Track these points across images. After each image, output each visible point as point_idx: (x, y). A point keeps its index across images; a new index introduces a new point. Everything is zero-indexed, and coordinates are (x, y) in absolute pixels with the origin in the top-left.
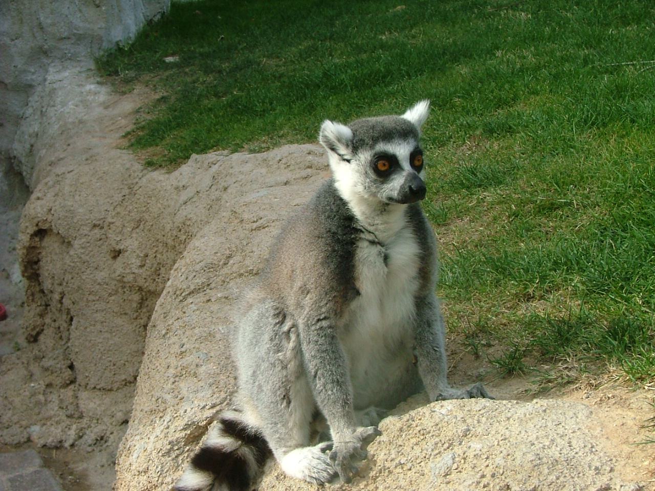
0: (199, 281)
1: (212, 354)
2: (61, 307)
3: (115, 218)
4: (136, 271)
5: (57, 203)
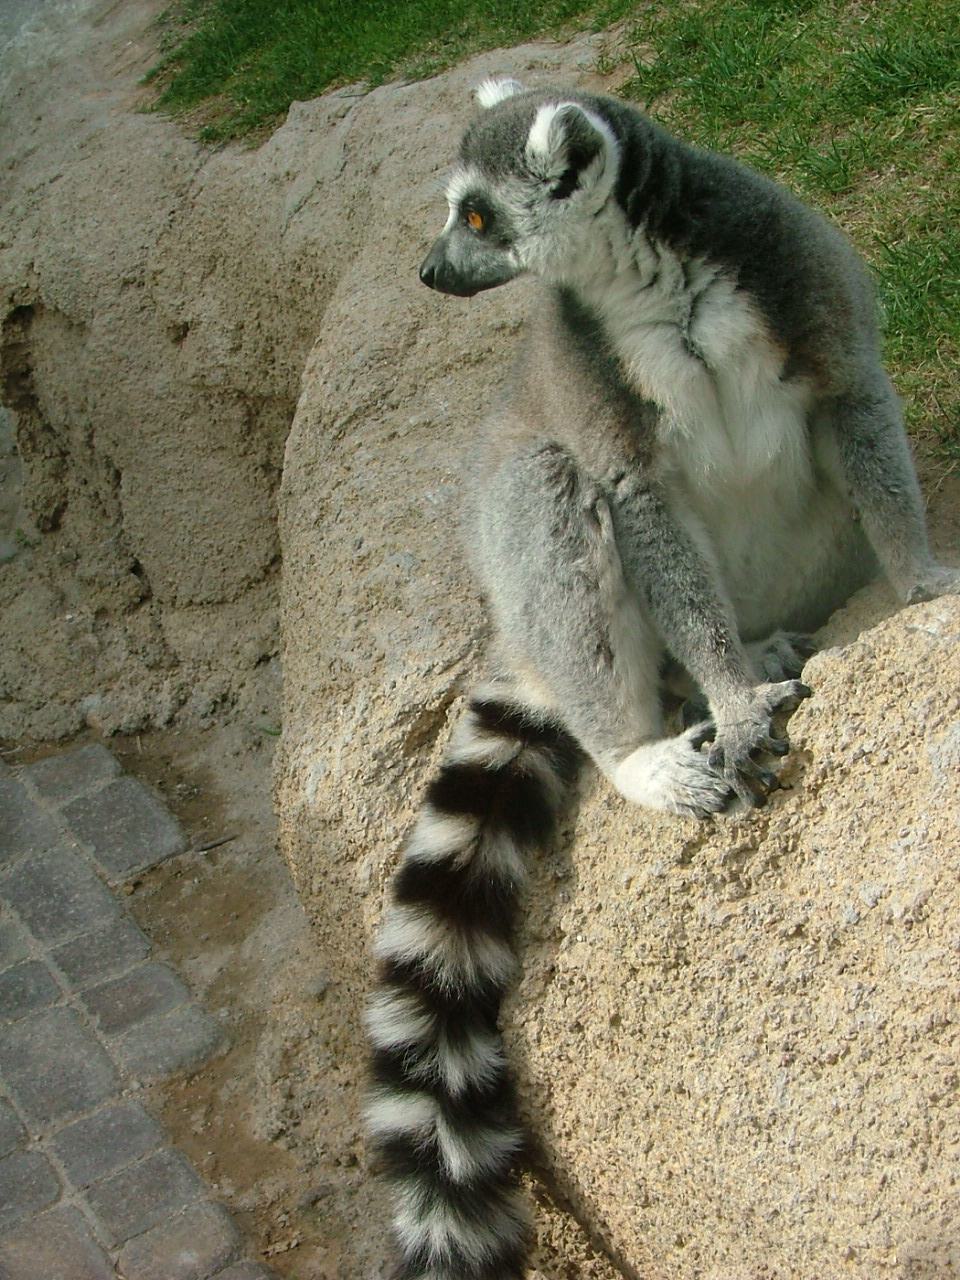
0: (364, 390)
1: (424, 554)
2: (93, 453)
3: (164, 260)
4: (227, 361)
5: (41, 249)
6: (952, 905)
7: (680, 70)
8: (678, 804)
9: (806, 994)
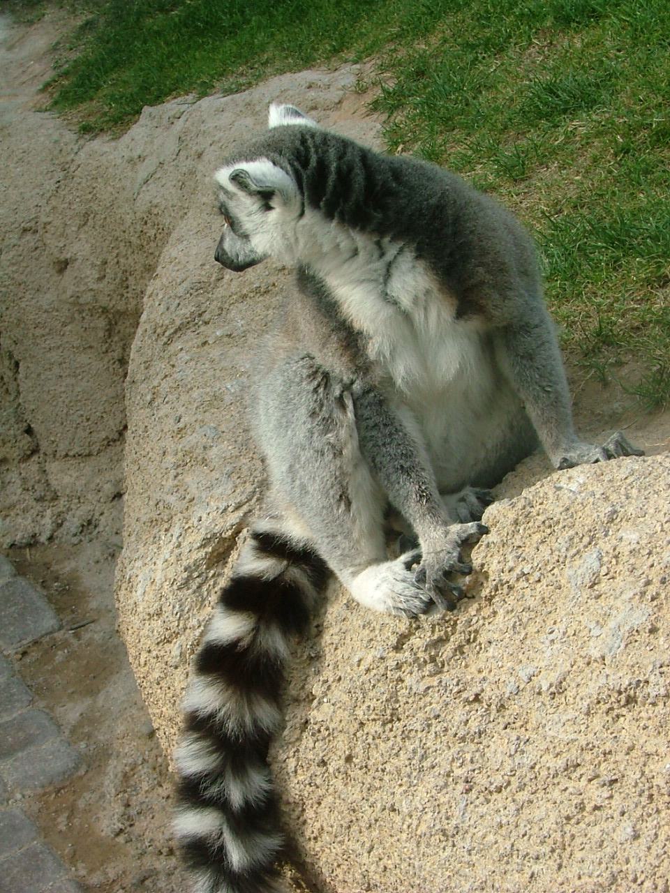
0: (186, 311)
1: (223, 428)
4: (95, 287)
6: (583, 682)
7: (412, 92)
8: (394, 608)
9: (481, 743)
